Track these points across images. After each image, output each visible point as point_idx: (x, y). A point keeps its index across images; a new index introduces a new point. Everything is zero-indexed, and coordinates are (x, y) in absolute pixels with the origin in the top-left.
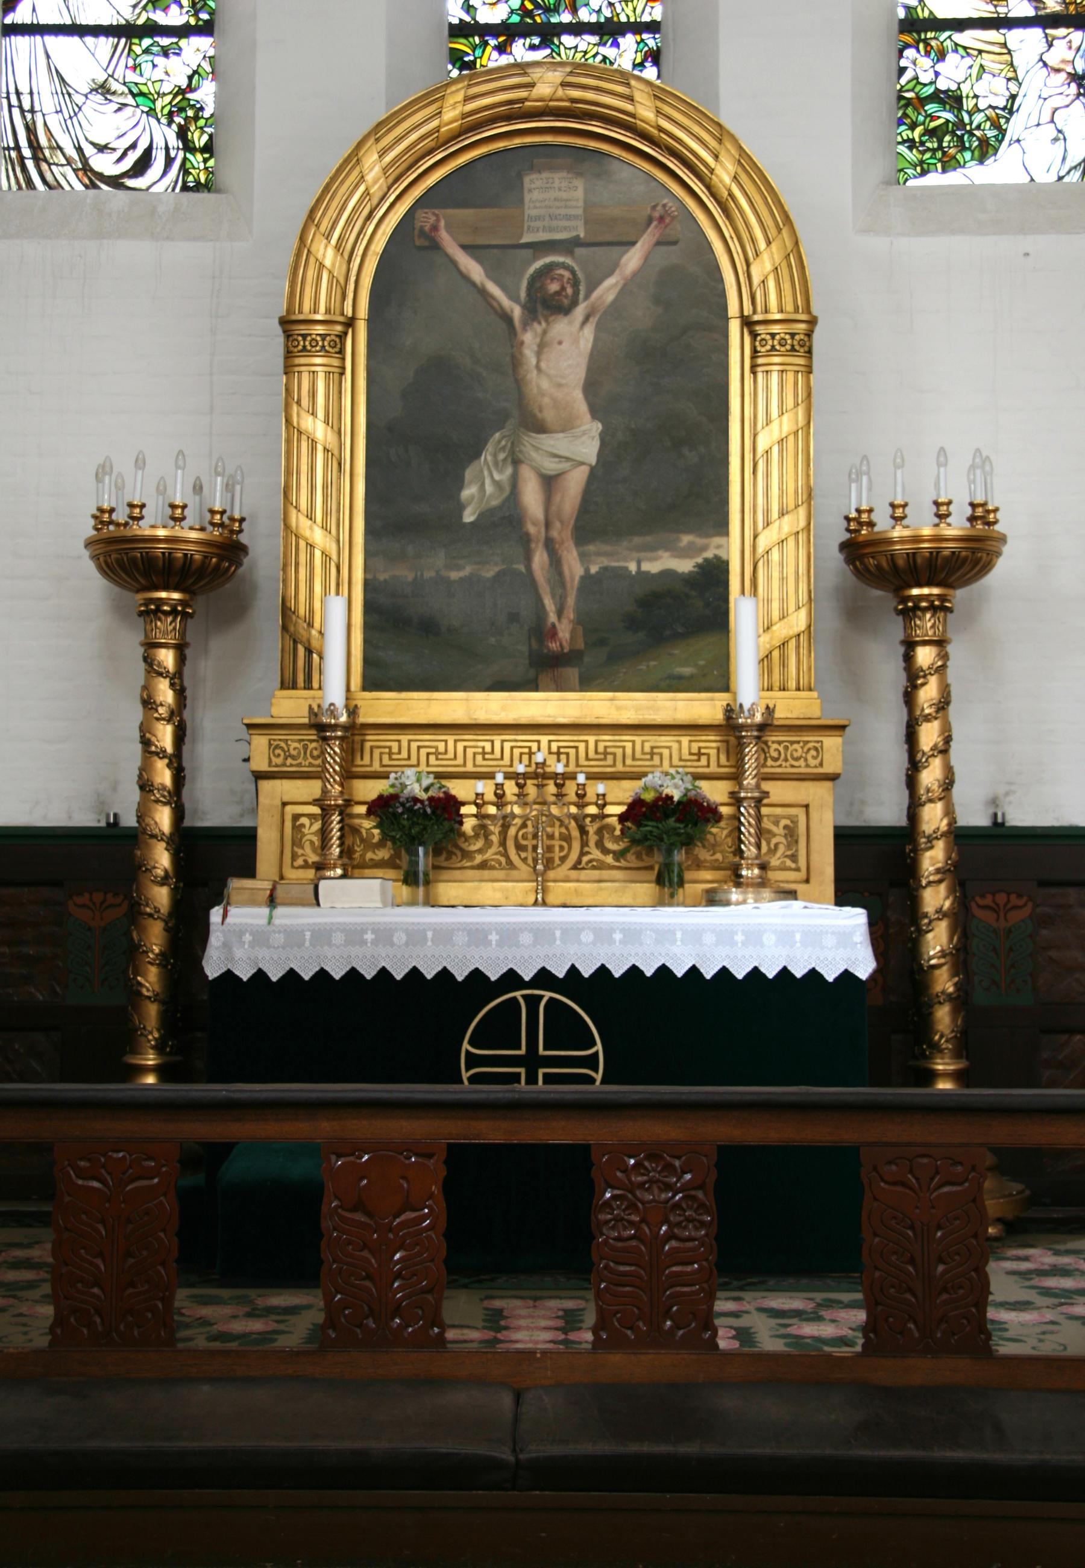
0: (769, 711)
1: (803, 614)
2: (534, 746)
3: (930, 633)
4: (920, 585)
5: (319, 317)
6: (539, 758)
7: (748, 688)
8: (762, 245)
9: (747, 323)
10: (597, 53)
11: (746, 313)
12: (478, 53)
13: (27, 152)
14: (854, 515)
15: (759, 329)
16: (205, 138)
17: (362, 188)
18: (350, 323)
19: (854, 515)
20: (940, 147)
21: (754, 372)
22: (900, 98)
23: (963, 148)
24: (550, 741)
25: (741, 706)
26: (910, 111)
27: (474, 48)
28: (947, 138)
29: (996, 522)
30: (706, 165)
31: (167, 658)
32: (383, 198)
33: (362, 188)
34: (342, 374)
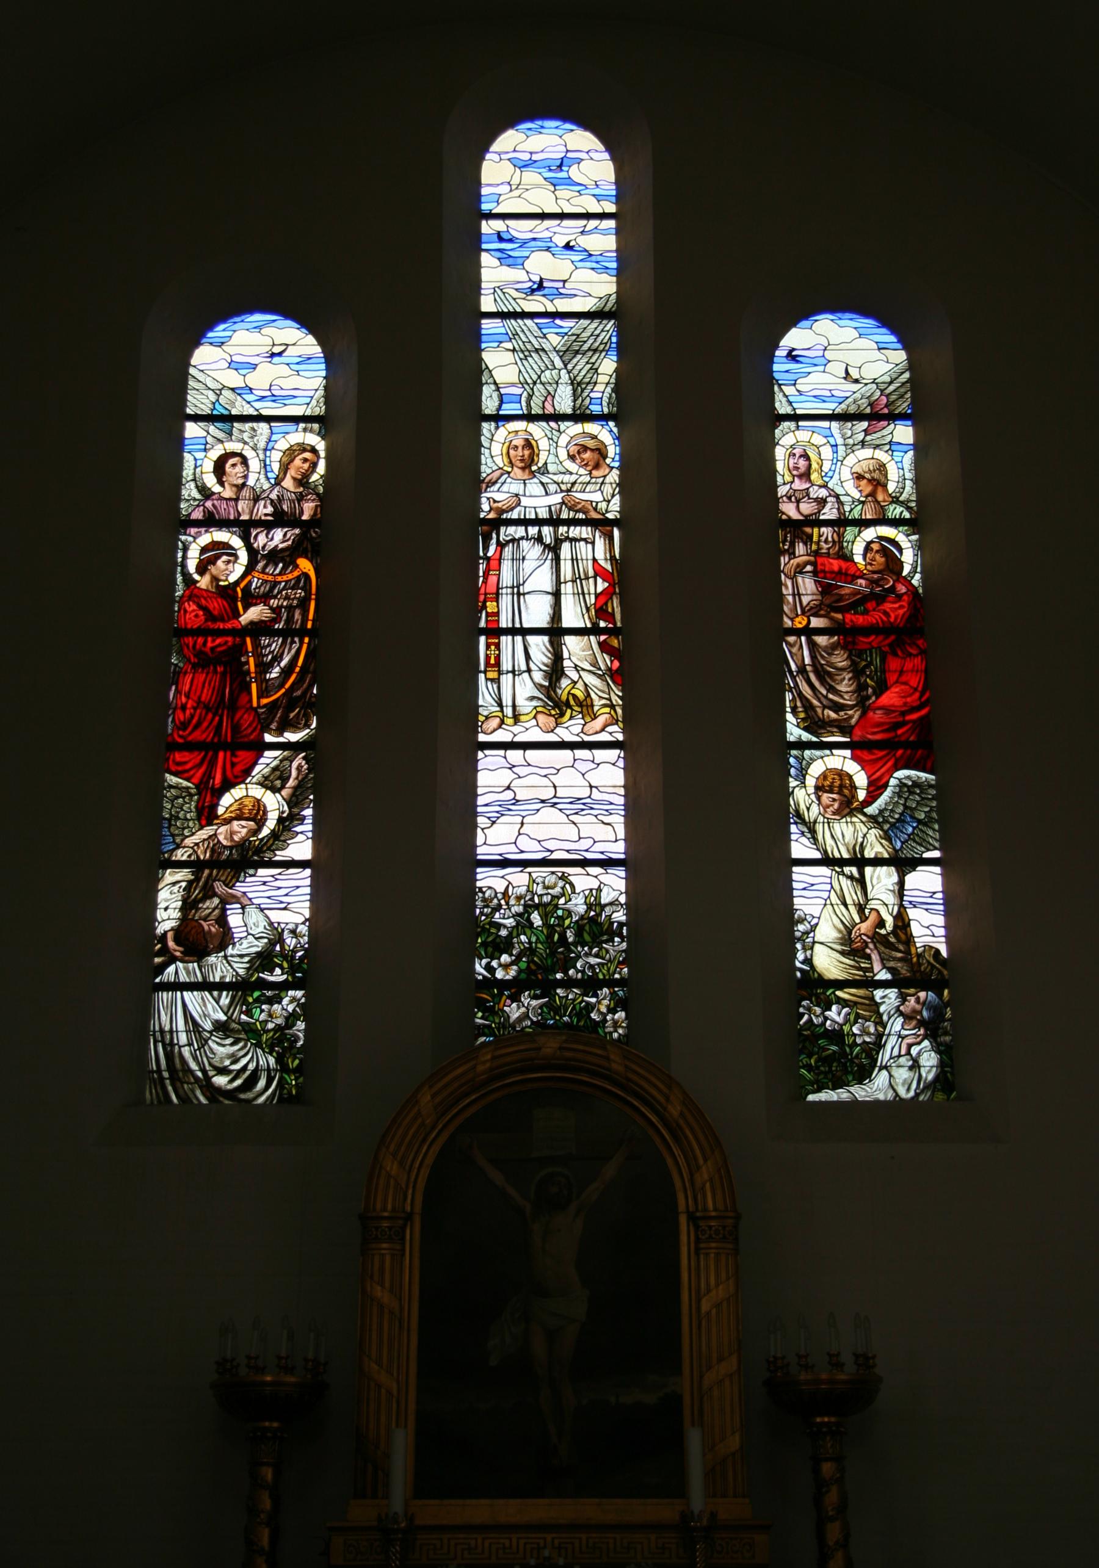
0: (713, 1515)
1: (737, 1437)
2: (542, 1542)
3: (831, 1451)
4: (822, 1415)
5: (386, 1214)
6: (546, 1553)
7: (697, 1500)
8: (701, 1161)
9: (692, 1218)
10: (583, 1001)
11: (691, 1209)
12: (496, 1000)
13: (166, 1074)
14: (772, 1359)
15: (701, 1223)
16: (297, 1062)
17: (419, 1121)
18: (409, 1217)
19: (772, 1359)
20: (830, 1071)
21: (697, 1253)
22: (801, 1035)
23: (846, 1073)
24: (553, 1539)
25: (692, 1512)
26: (807, 1044)
27: (493, 996)
28: (835, 1064)
29: (874, 1366)
30: (660, 1104)
31: (268, 1474)
32: (433, 1128)
33: (419, 1121)
34: (403, 1255)
